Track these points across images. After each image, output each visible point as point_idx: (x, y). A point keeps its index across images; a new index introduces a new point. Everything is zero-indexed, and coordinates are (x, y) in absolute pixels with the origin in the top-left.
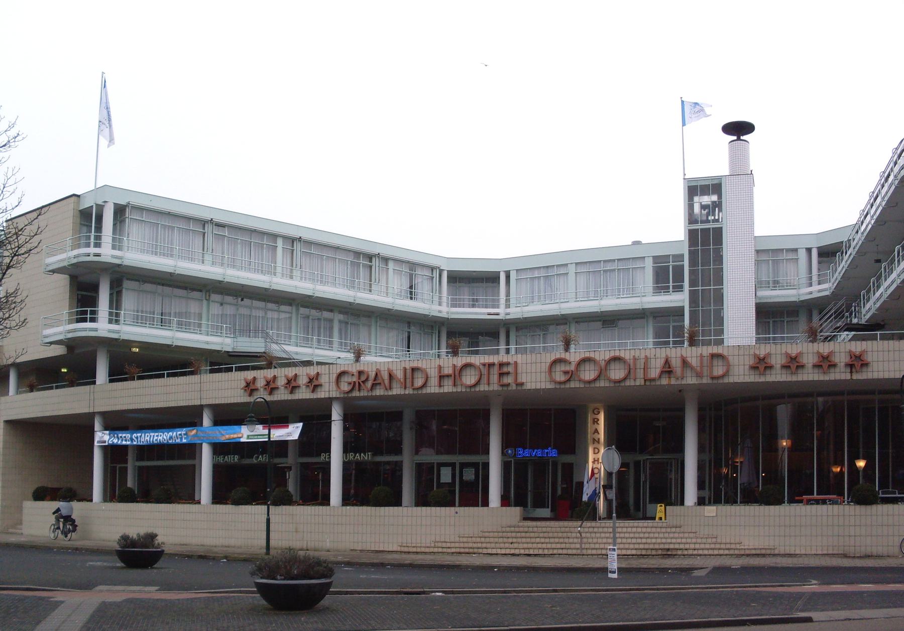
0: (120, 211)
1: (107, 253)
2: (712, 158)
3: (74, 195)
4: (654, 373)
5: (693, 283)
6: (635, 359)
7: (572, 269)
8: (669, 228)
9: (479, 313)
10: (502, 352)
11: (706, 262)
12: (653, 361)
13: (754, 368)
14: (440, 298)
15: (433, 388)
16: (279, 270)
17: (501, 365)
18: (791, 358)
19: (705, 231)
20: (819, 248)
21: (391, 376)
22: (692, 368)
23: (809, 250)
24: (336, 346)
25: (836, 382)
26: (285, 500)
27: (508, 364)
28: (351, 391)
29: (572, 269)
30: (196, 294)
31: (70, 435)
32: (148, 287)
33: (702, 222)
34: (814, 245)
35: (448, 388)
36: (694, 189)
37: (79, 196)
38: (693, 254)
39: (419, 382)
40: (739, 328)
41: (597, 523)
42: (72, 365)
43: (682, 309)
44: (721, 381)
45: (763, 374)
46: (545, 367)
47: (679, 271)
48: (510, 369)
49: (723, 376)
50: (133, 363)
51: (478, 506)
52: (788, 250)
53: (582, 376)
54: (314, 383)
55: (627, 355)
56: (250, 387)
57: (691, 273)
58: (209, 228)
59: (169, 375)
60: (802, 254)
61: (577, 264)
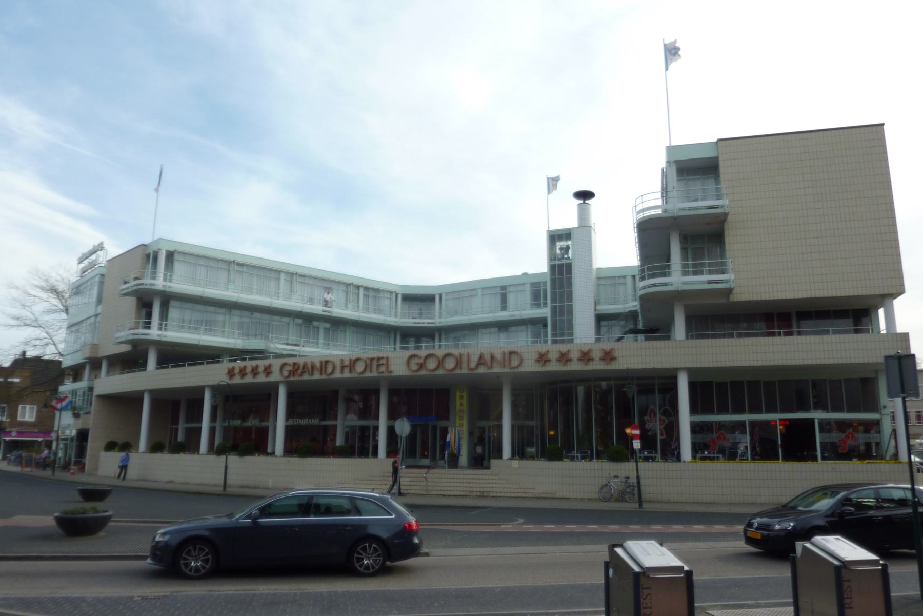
0: (170, 256)
1: (160, 283)
2: (566, 216)
4: (473, 364)
5: (554, 300)
6: (461, 355)
7: (480, 292)
8: (537, 263)
9: (425, 322)
10: (437, 347)
11: (561, 287)
13: (538, 361)
14: (396, 313)
15: (337, 375)
17: (379, 359)
19: (561, 266)
21: (492, 358)
24: (321, 345)
25: (593, 371)
27: (383, 358)
29: (480, 292)
30: (223, 310)
31: (126, 403)
33: (559, 259)
35: (346, 375)
36: (555, 237)
37: (145, 245)
38: (553, 281)
39: (330, 370)
40: (584, 331)
42: (131, 360)
43: (545, 319)
44: (516, 371)
45: (565, 365)
46: (405, 360)
50: (174, 355)
52: (619, 277)
54: (268, 371)
55: (456, 352)
56: (231, 373)
58: (232, 265)
59: (208, 363)
61: (483, 289)
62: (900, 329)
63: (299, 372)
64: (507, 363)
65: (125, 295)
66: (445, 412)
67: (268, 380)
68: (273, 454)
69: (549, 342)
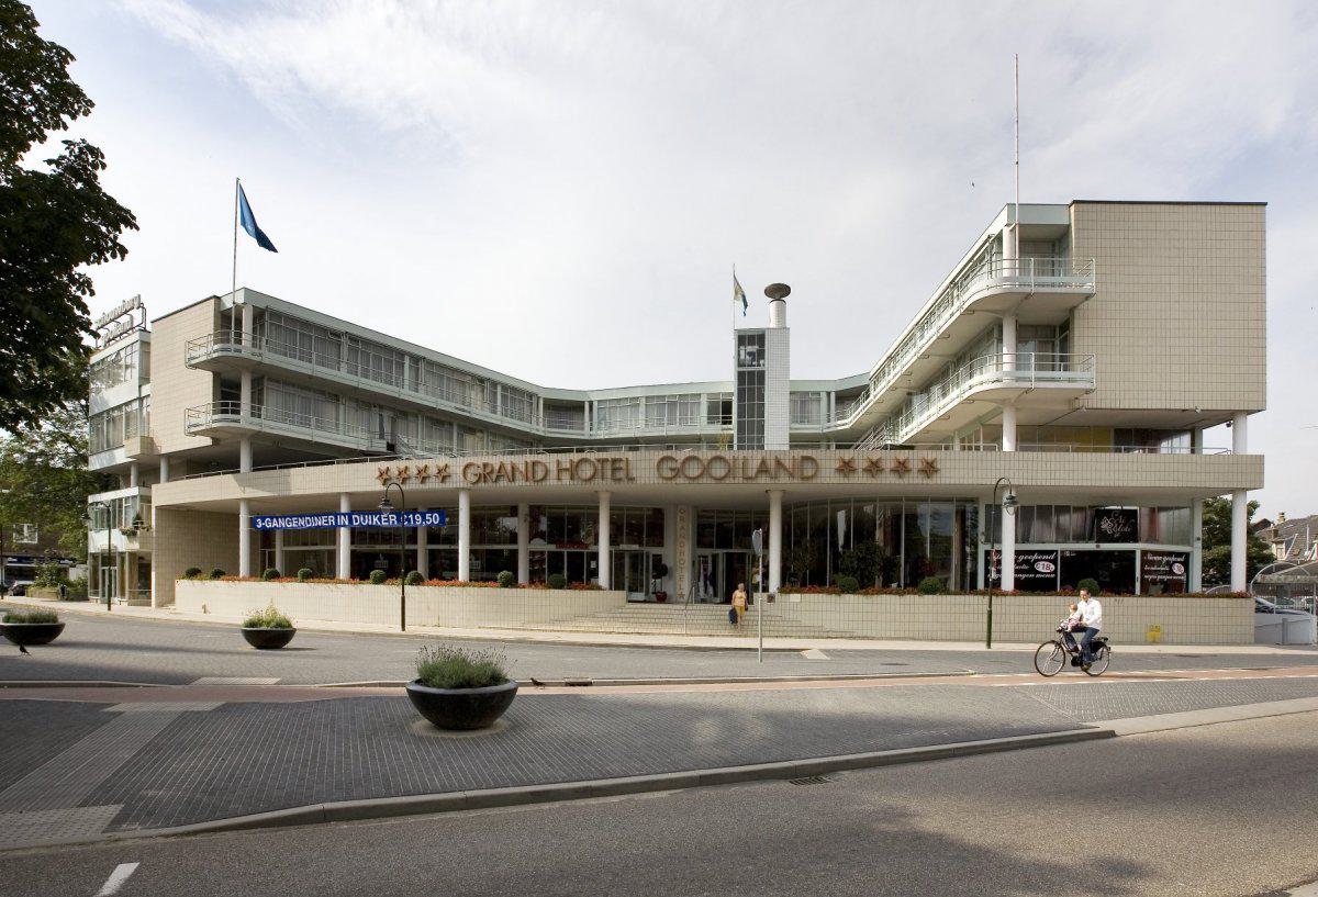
3: (215, 296)
5: (740, 415)
6: (735, 459)
12: (750, 462)
13: (839, 470)
14: (538, 419)
15: (552, 482)
16: (406, 382)
17: (615, 461)
18: (872, 463)
20: (836, 392)
21: (778, 462)
22: (785, 469)
23: (829, 394)
26: (418, 581)
27: (620, 460)
28: (477, 482)
31: (219, 520)
32: (291, 390)
34: (833, 388)
36: (744, 339)
38: (741, 392)
39: (540, 475)
40: (777, 432)
41: (519, 591)
47: (727, 407)
48: (623, 465)
49: (812, 477)
51: (1132, 593)
53: (687, 473)
57: (739, 407)
60: (824, 396)
62: (1252, 450)
63: (494, 476)
64: (530, 475)
65: (195, 366)
66: (623, 558)
67: (422, 487)
68: (994, 587)
69: (735, 448)
